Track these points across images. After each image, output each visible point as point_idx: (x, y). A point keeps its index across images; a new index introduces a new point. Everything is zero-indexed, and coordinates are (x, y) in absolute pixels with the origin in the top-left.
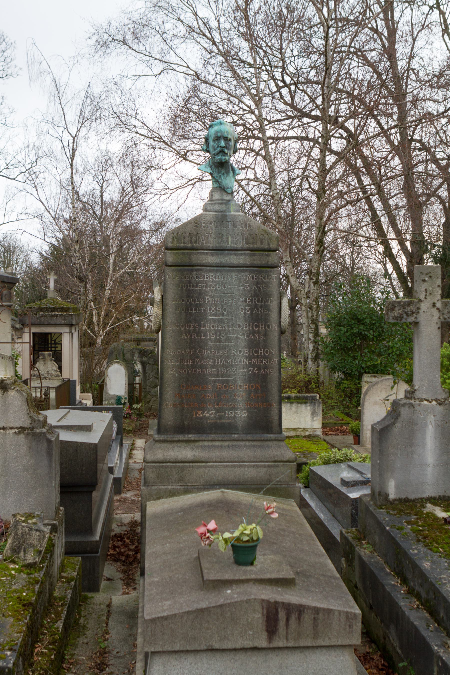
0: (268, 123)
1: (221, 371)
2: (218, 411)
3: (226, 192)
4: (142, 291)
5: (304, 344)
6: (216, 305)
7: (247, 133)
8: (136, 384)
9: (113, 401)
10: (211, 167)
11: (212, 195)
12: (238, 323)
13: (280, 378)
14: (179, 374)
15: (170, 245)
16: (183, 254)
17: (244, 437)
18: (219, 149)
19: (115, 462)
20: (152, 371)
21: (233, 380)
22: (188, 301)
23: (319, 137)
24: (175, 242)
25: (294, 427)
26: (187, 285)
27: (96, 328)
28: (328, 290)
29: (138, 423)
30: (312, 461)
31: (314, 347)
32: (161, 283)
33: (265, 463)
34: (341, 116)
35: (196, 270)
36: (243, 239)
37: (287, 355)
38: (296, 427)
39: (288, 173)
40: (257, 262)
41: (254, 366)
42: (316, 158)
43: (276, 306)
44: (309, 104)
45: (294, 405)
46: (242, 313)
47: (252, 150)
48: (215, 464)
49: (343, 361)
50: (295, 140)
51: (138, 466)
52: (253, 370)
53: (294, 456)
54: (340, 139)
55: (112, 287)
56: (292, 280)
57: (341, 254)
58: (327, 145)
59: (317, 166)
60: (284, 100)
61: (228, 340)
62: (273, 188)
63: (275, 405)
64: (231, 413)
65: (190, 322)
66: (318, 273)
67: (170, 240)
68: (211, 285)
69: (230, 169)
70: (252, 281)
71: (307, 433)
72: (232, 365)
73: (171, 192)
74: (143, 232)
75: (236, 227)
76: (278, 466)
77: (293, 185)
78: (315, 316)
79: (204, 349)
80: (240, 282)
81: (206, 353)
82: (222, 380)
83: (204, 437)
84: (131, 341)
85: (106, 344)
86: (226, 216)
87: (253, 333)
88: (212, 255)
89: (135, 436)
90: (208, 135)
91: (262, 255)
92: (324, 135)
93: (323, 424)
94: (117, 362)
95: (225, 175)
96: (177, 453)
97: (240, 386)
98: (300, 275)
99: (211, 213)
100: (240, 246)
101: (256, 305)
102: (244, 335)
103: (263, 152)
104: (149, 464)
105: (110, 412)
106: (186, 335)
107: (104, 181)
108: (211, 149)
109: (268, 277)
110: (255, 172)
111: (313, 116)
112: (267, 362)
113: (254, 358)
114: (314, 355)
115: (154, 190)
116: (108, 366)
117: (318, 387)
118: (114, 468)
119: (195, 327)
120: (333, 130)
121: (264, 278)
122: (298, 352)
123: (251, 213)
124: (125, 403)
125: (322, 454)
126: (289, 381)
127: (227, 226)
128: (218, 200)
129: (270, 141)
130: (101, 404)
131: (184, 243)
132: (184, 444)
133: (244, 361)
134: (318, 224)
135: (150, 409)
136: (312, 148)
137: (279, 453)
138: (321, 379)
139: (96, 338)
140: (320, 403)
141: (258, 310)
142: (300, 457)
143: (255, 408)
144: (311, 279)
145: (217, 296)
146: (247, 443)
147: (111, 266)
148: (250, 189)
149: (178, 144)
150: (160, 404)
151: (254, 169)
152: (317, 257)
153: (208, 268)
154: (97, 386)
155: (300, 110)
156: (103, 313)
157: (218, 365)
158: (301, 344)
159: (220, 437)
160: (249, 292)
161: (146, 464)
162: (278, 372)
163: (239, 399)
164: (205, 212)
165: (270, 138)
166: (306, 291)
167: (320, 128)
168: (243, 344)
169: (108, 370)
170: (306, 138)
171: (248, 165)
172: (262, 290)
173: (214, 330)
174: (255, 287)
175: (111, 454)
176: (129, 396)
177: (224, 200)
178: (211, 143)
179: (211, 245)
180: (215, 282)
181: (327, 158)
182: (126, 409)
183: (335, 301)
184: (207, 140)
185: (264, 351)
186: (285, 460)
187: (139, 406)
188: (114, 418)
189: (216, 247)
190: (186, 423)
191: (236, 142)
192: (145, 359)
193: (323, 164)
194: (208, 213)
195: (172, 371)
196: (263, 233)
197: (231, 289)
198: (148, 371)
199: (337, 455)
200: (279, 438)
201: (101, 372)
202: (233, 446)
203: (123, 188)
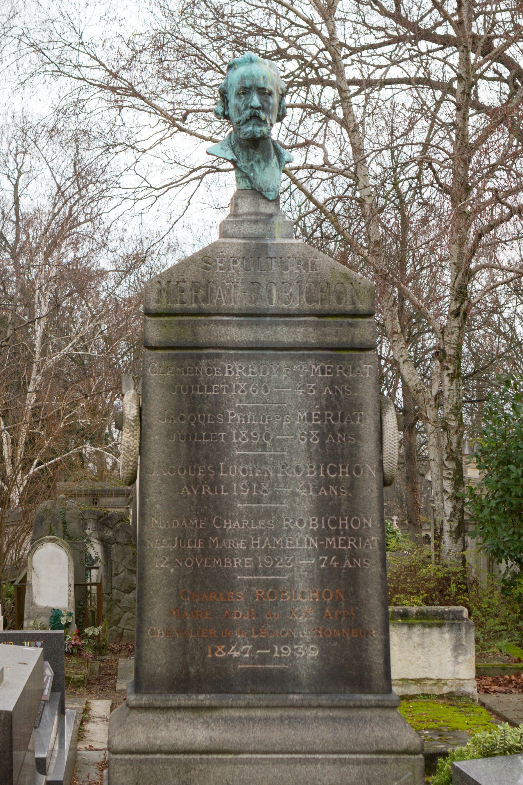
0: (348, 52)
1: (263, 562)
2: (258, 645)
3: (265, 198)
4: (100, 394)
5: (433, 501)
6: (249, 428)
7: (307, 75)
8: (91, 584)
9: (45, 620)
10: (233, 149)
11: (236, 205)
12: (295, 463)
13: (383, 578)
14: (176, 569)
15: (153, 306)
16: (180, 323)
17: (314, 700)
18: (248, 112)
19: (50, 748)
20: (124, 558)
21: (288, 580)
22: (192, 419)
23: (452, 80)
24: (164, 299)
25: (418, 677)
26: (190, 388)
27: (9, 470)
28: (480, 389)
29: (96, 666)
30: (458, 749)
31: (454, 507)
32: (138, 378)
33: (358, 756)
34: (496, 37)
35: (208, 356)
36: (301, 293)
37: (401, 524)
38: (422, 676)
39: (392, 153)
40: (332, 339)
41: (330, 552)
42: (450, 121)
43: (372, 429)
44: (430, 11)
45: (417, 630)
46: (302, 443)
47: (316, 108)
48: (254, 756)
49: (516, 537)
50: (405, 86)
51: (98, 757)
52: (329, 560)
53: (417, 741)
54: (496, 83)
55: (40, 386)
56: (406, 369)
57: (506, 315)
58: (469, 95)
59: (451, 139)
60: (380, 6)
61: (275, 498)
62: (361, 185)
63: (376, 634)
64: (285, 649)
65: (198, 461)
66: (458, 357)
67: (153, 296)
68: (238, 387)
69: (272, 151)
70: (322, 379)
71: (446, 690)
72: (284, 551)
73: (156, 193)
74: (102, 274)
75: (286, 269)
76: (385, 762)
77: (402, 177)
78: (454, 445)
79: (227, 518)
80: (298, 379)
81: (231, 526)
82: (264, 581)
83: (230, 699)
84: (79, 495)
85: (29, 502)
86: (266, 246)
87: (327, 483)
88: (240, 325)
89: (91, 693)
90: (226, 85)
91: (341, 326)
92: (464, 76)
93: (477, 669)
94: (51, 540)
95: (263, 164)
96: (175, 734)
97: (303, 593)
98: (422, 359)
99: (235, 240)
100: (295, 306)
101: (331, 428)
102: (308, 488)
103: (340, 112)
104: (119, 757)
105: (39, 643)
106: (190, 488)
107: (20, 174)
108: (232, 112)
109: (353, 368)
110: (325, 152)
111: (440, 36)
112: (357, 544)
113: (330, 536)
114: (455, 524)
115: (121, 191)
116: (34, 548)
117: (466, 591)
118: (48, 761)
119: (207, 472)
120: (481, 64)
121: (346, 371)
122: (422, 518)
123: (318, 234)
124: (68, 625)
125: (478, 735)
126: (405, 580)
127: (269, 267)
128: (249, 214)
129: (354, 89)
130: (21, 627)
131: (182, 302)
132: (188, 715)
133: (308, 541)
134: (455, 255)
135: (121, 636)
136: (438, 104)
137: (386, 735)
138: (472, 574)
139: (10, 491)
140: (470, 626)
141: (335, 436)
142: (431, 740)
143: (335, 639)
144: (445, 368)
145: (251, 409)
146: (320, 713)
147: (37, 343)
148: (314, 186)
149: (169, 97)
150: (140, 631)
151: (322, 146)
152: (455, 323)
153: (232, 352)
154: (12, 589)
155: (413, 26)
156: (22, 439)
157: (255, 551)
158: (429, 500)
159: (264, 699)
160: (316, 399)
161: (112, 756)
162: (379, 564)
163: (301, 620)
164: (223, 240)
165: (353, 82)
166: (434, 393)
167: (455, 59)
168: (306, 506)
169: (34, 557)
170: (427, 82)
171: (310, 138)
172: (342, 397)
173: (247, 478)
174: (327, 391)
175: (41, 731)
176: (77, 610)
177: (262, 214)
178: (233, 101)
179: (236, 306)
180: (246, 380)
181: (471, 121)
182: (71, 637)
183: (496, 413)
184: (223, 94)
185: (349, 521)
186: (400, 748)
187: (97, 631)
188: (46, 656)
189: (247, 309)
190: (192, 670)
191: (282, 96)
192: (109, 534)
193: (462, 136)
194: (228, 240)
195: (161, 562)
196: (342, 280)
197: (279, 394)
198: (115, 559)
199: (509, 738)
200: (387, 703)
201: (19, 560)
202: (290, 718)
203: (59, 188)
